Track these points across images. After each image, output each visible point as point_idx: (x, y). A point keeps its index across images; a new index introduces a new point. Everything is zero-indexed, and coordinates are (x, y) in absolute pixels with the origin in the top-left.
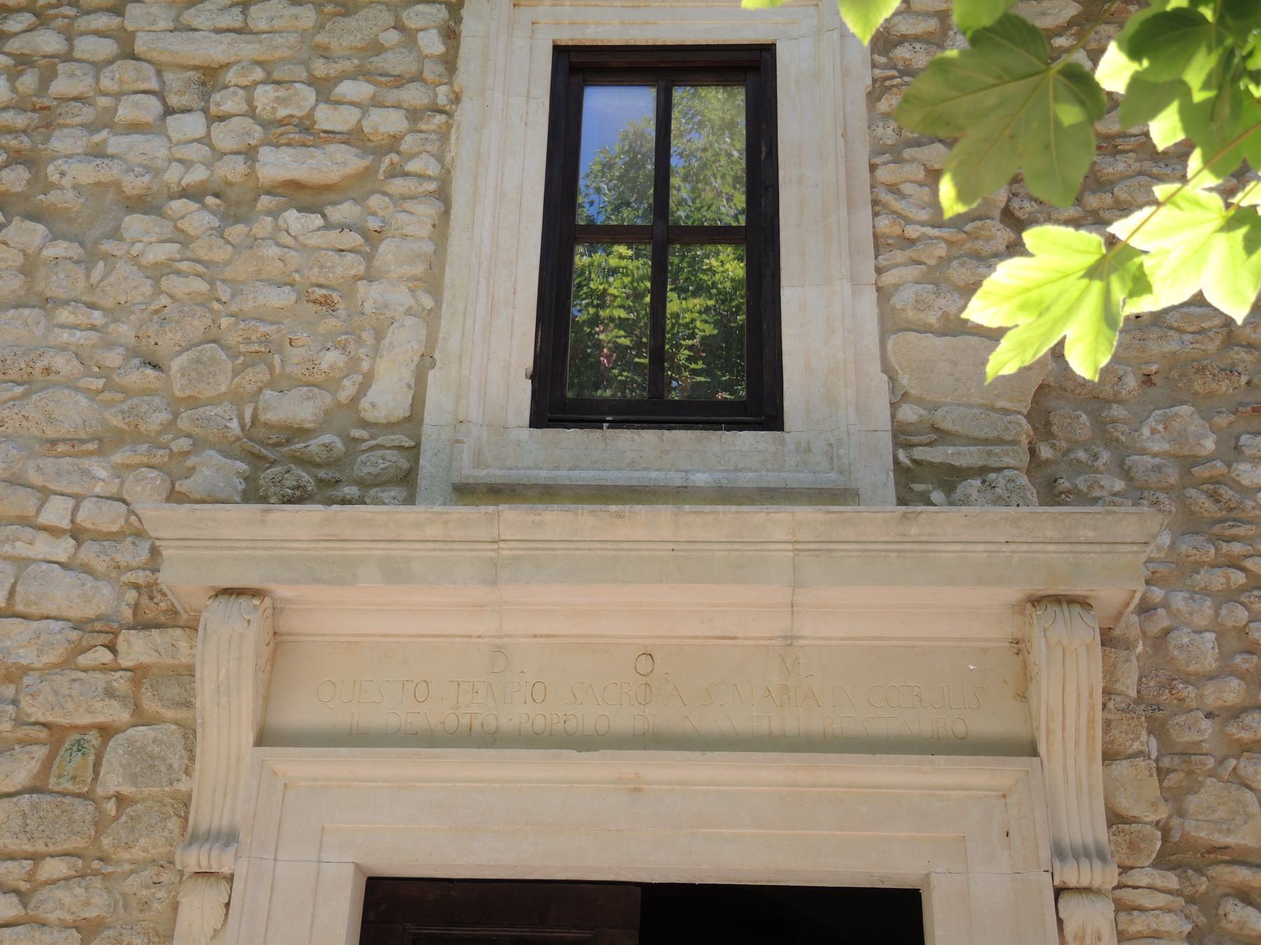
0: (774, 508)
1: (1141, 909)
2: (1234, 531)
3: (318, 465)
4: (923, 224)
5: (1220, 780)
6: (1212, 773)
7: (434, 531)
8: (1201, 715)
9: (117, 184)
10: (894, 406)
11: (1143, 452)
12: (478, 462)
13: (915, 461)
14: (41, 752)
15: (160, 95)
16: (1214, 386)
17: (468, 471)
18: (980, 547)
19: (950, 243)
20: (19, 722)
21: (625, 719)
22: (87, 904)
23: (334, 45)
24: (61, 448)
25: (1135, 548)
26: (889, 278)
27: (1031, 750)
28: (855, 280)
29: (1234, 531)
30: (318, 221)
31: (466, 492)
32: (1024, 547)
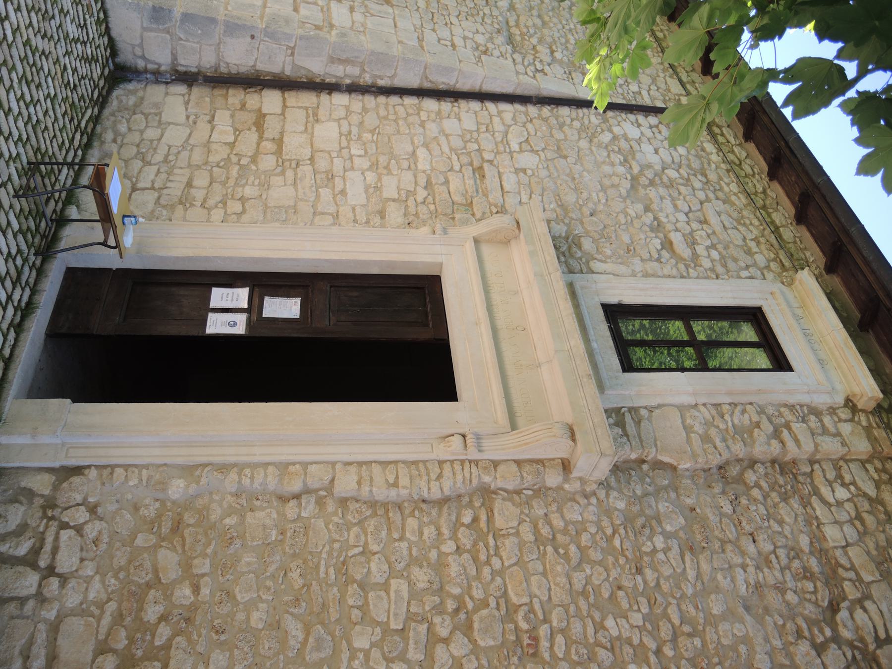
0: (581, 338)
1: (463, 469)
2: (630, 531)
3: (569, 252)
4: (732, 421)
5: (520, 514)
6: (522, 512)
7: (548, 258)
8: (546, 511)
9: (652, 203)
10: (645, 408)
11: (657, 502)
12: (582, 288)
13: (624, 414)
14: (464, 202)
15: (690, 210)
16: (697, 532)
17: (577, 287)
18: (585, 402)
19: (727, 430)
20: (472, 197)
21: (500, 323)
22: (423, 214)
23: (731, 249)
24: (557, 197)
25: (598, 449)
26: (702, 408)
27: (514, 426)
28: (695, 394)
29: (630, 531)
30: (659, 247)
31: (571, 289)
32: (589, 415)
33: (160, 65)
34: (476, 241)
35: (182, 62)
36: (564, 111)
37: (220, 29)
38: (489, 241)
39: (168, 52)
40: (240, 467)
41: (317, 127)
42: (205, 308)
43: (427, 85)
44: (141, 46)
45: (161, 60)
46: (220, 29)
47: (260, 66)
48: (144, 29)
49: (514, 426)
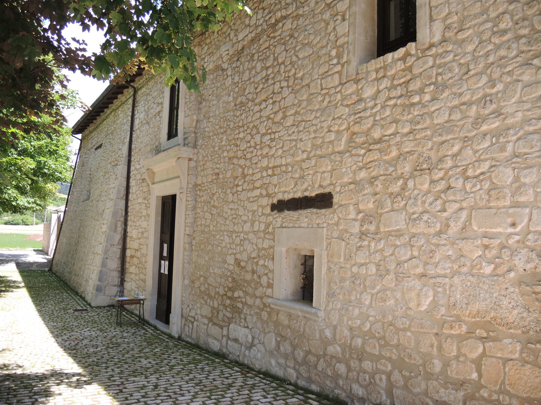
27: (179, 177)
33: (118, 291)
34: (153, 184)
35: (117, 283)
36: (133, 146)
37: (104, 269)
38: (153, 179)
39: (113, 288)
40: (184, 263)
41: (134, 237)
42: (164, 274)
43: (125, 198)
44: (111, 296)
45: (116, 291)
46: (104, 269)
47: (118, 256)
48: (104, 295)
49: (179, 177)
